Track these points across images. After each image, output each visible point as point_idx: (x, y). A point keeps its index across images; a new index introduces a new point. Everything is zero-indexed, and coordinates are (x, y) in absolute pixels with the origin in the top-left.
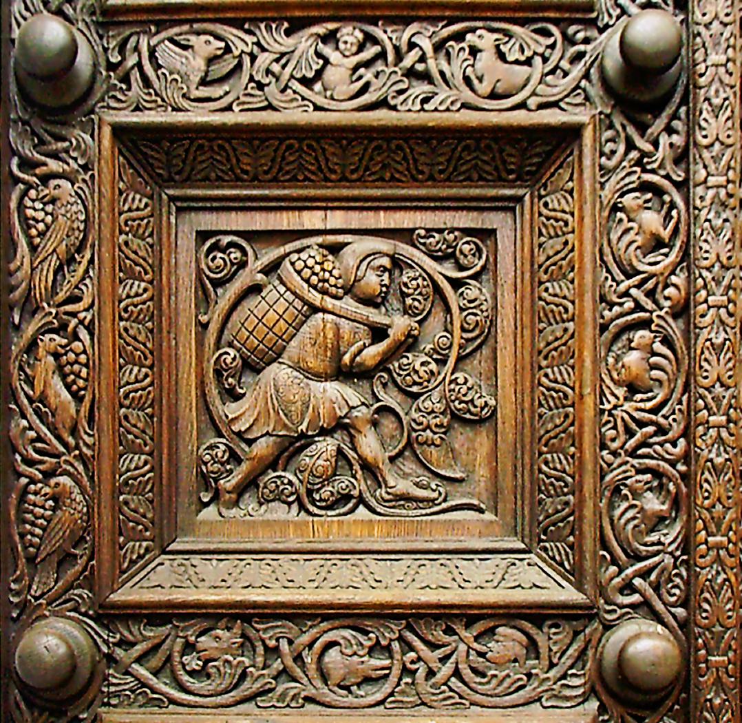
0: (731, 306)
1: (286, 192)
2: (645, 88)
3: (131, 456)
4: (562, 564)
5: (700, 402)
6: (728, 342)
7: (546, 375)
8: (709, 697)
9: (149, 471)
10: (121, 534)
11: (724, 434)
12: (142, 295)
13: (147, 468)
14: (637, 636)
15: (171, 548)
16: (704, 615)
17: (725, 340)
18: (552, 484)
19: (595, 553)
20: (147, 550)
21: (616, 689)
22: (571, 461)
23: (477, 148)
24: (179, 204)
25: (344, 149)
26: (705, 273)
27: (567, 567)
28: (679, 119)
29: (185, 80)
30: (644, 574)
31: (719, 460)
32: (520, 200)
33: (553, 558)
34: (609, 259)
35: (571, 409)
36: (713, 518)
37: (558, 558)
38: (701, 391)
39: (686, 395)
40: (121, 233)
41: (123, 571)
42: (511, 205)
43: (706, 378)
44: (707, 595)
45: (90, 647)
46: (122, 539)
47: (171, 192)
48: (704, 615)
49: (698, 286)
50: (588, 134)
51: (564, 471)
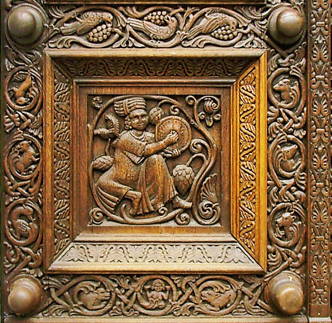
1: (133, 80)
2: (282, 41)
3: (61, 83)
5: (312, 121)
6: (325, 42)
7: (243, 88)
8: (316, 254)
9: (68, 91)
12: (65, 206)
13: (67, 205)
14: (279, 17)
16: (314, 217)
17: (324, 41)
20: (67, 241)
21: (275, 37)
23: (215, 65)
26: (315, 12)
27: (253, 250)
29: (91, 37)
31: (320, 42)
32: (232, 83)
36: (318, 13)
38: (312, 224)
39: (306, 108)
41: (54, 255)
42: (229, 86)
43: (315, 57)
44: (315, 155)
45: (36, 288)
48: (314, 271)
49: (312, 124)
50: (263, 59)
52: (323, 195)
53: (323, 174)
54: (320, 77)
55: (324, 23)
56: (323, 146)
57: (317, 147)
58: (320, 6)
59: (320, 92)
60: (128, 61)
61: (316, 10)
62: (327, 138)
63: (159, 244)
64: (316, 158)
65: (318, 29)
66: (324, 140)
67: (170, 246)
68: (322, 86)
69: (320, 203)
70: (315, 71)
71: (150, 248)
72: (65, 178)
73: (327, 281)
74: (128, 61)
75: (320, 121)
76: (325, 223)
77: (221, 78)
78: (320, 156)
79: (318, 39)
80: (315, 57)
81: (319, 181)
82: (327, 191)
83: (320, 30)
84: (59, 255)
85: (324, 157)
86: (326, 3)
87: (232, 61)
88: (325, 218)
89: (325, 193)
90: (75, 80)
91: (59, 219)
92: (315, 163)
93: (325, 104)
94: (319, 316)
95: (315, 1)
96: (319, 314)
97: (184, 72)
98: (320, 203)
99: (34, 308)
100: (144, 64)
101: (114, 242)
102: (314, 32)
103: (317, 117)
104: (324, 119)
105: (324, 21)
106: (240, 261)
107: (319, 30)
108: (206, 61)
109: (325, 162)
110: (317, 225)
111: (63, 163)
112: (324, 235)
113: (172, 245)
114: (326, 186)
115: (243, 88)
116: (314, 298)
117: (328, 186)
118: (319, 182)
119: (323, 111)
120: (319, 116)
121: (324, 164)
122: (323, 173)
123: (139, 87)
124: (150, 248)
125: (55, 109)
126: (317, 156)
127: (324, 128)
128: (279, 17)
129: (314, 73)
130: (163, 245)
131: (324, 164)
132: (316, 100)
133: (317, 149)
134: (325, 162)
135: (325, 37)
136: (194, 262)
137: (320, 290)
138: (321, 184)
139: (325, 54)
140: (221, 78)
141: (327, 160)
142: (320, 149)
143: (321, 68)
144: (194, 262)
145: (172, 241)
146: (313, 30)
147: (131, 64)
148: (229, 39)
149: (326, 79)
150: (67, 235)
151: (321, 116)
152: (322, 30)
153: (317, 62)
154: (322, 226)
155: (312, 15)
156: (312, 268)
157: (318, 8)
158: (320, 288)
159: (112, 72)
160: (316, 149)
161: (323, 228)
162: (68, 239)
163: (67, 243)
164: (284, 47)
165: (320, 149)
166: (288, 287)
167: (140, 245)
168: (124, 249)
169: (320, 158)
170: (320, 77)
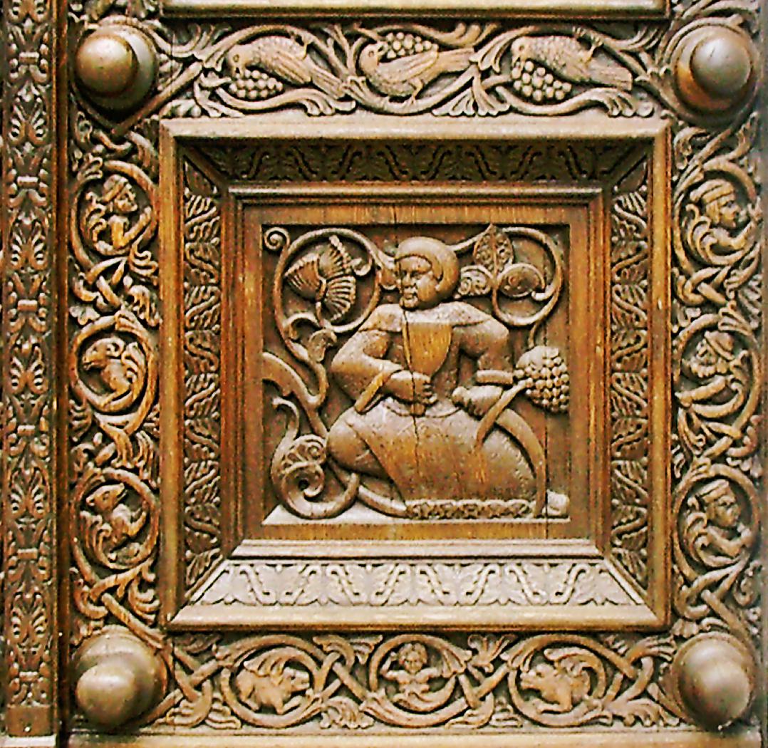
0: (43, 62)
2: (712, 106)
4: (634, 576)
6: (39, 100)
10: (188, 547)
11: (36, 197)
13: (213, 472)
14: (702, 43)
15: (236, 552)
18: (623, 226)
19: (666, 436)
22: (644, 295)
24: (245, 201)
25: (324, 156)
28: (752, 425)
30: (713, 586)
31: (28, 99)
32: (592, 196)
33: (626, 568)
34: (681, 254)
35: (644, 332)
37: (630, 207)
40: (186, 241)
44: (15, 360)
46: (186, 460)
47: (235, 190)
51: (636, 305)
52: (34, 454)
53: (33, 405)
54: (28, 179)
55: (36, 55)
56: (34, 341)
57: (19, 342)
58: (28, 16)
59: (28, 215)
60: (349, 147)
61: (19, 25)
62: (43, 323)
63: (508, 561)
64: (18, 369)
65: (22, 70)
66: (34, 325)
67: (446, 568)
68: (31, 201)
69: (28, 472)
70: (14, 166)
71: (492, 572)
72: (208, 415)
73: (47, 652)
74: (349, 147)
75: (27, 281)
76: (39, 520)
77: (243, 184)
78: (27, 364)
79: (23, 92)
80: (15, 135)
81: (25, 421)
82: (44, 444)
83: (28, 72)
84: (198, 588)
85: (35, 364)
86: (41, 9)
87: (497, 148)
88: (39, 508)
89: (39, 449)
90: (231, 190)
91: (195, 503)
92: (15, 381)
93: (39, 241)
94: (29, 734)
95: (17, 5)
96: (27, 729)
97: (391, 171)
98: (28, 472)
99: (142, 710)
100: (297, 155)
101: (356, 558)
102: (15, 75)
103: (20, 275)
104: (36, 277)
105: (38, 51)
106: (607, 600)
107: (24, 72)
108: (440, 147)
109: (39, 376)
110: (20, 523)
111: (205, 379)
112: (38, 547)
113: (538, 565)
114: (42, 433)
115: (620, 203)
116: (17, 693)
117: (46, 433)
118: (25, 424)
119: (32, 257)
120: (23, 271)
121: (36, 381)
122: (33, 402)
123: (303, 204)
124: (492, 572)
125: (185, 259)
126: (19, 363)
127: (37, 299)
128: (702, 43)
129: (14, 172)
130: (341, 565)
131: (36, 381)
132: (19, 234)
133: (20, 347)
134: (39, 376)
135: (39, 87)
136: (596, 603)
137: (29, 674)
138: (30, 428)
139: (39, 127)
140: (562, 185)
141: (44, 373)
142: (26, 347)
143: (27, 159)
144: (596, 603)
145: (507, 554)
146: (13, 71)
147: (449, 153)
148: (247, 99)
149: (42, 185)
150: (215, 540)
151: (29, 269)
152: (32, 71)
153: (20, 146)
154: (33, 526)
155: (11, 37)
156: (11, 623)
157: (24, 21)
158: (29, 670)
159: (406, 173)
160: (17, 349)
161: (34, 530)
162: (217, 550)
163: (215, 562)
164: (118, 116)
165: (26, 347)
166: (717, 663)
167: (469, 565)
168: (253, 576)
169: (26, 369)
170: (28, 179)
